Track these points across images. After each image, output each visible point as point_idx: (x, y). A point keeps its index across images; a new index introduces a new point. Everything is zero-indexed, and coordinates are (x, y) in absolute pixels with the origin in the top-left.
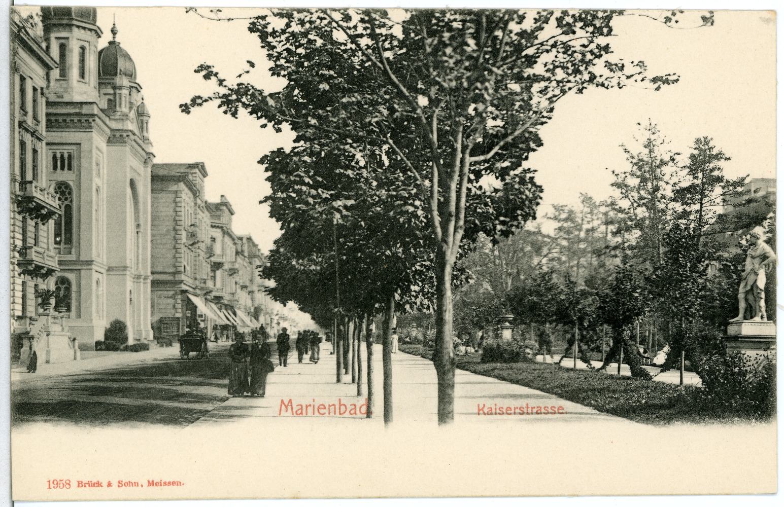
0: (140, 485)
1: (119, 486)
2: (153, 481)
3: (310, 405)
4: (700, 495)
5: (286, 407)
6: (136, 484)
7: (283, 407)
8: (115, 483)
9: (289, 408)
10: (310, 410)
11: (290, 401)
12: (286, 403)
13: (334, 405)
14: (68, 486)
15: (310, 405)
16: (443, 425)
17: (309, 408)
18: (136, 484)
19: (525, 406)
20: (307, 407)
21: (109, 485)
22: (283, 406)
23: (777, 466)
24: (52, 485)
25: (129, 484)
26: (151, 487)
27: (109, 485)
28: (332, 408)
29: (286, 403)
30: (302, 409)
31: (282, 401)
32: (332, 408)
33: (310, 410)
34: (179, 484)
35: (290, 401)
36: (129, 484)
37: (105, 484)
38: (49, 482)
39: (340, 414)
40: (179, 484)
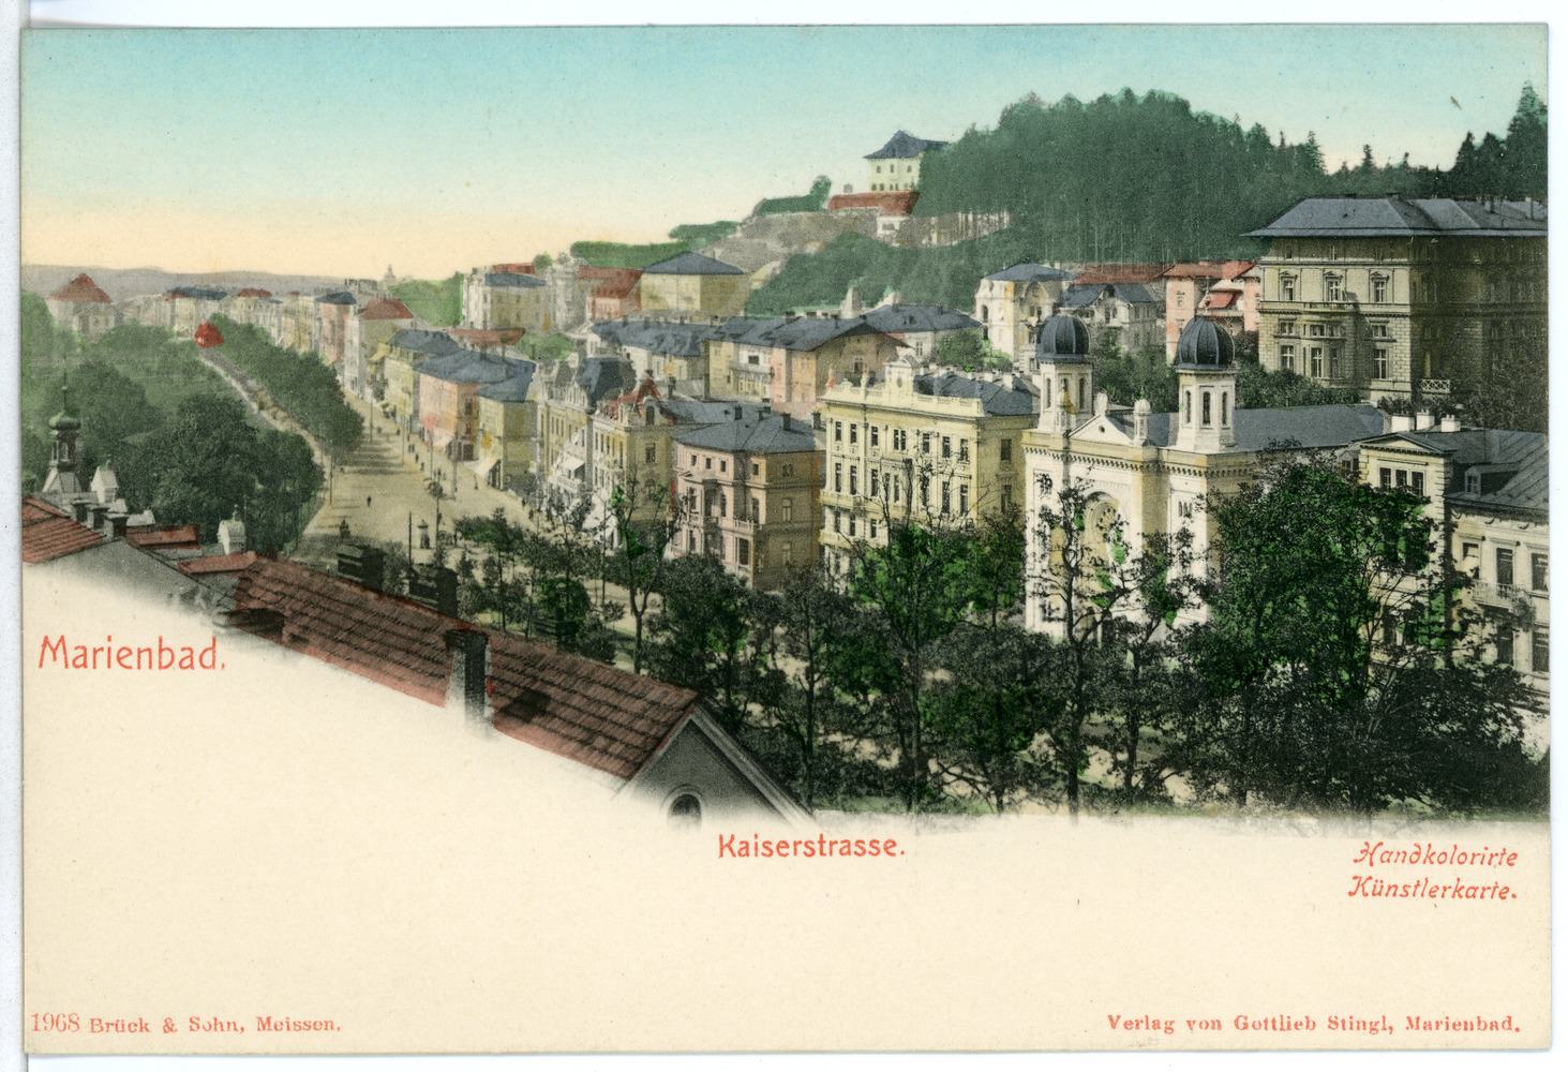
0: (335, 1027)
1: (192, 1029)
2: (268, 1019)
3: (102, 649)
4: (1256, 1051)
5: (54, 651)
6: (232, 1025)
7: (48, 652)
8: (181, 1024)
9: (60, 652)
10: (102, 657)
11: (62, 639)
12: (54, 644)
13: (149, 650)
14: (73, 1027)
15: (102, 649)
16: (679, 819)
17: (99, 654)
18: (232, 1025)
19: (816, 839)
20: (95, 651)
21: (169, 1027)
22: (48, 652)
23: (1550, 958)
24: (41, 1025)
25: (216, 1025)
26: (1413, 1031)
27: (169, 1027)
28: (145, 656)
29: (54, 644)
30: (85, 655)
31: (46, 642)
32: (145, 656)
33: (102, 657)
34: (328, 1025)
35: (62, 639)
36: (216, 1025)
37: (156, 1025)
38: (36, 1016)
39: (160, 667)
40: (328, 1025)
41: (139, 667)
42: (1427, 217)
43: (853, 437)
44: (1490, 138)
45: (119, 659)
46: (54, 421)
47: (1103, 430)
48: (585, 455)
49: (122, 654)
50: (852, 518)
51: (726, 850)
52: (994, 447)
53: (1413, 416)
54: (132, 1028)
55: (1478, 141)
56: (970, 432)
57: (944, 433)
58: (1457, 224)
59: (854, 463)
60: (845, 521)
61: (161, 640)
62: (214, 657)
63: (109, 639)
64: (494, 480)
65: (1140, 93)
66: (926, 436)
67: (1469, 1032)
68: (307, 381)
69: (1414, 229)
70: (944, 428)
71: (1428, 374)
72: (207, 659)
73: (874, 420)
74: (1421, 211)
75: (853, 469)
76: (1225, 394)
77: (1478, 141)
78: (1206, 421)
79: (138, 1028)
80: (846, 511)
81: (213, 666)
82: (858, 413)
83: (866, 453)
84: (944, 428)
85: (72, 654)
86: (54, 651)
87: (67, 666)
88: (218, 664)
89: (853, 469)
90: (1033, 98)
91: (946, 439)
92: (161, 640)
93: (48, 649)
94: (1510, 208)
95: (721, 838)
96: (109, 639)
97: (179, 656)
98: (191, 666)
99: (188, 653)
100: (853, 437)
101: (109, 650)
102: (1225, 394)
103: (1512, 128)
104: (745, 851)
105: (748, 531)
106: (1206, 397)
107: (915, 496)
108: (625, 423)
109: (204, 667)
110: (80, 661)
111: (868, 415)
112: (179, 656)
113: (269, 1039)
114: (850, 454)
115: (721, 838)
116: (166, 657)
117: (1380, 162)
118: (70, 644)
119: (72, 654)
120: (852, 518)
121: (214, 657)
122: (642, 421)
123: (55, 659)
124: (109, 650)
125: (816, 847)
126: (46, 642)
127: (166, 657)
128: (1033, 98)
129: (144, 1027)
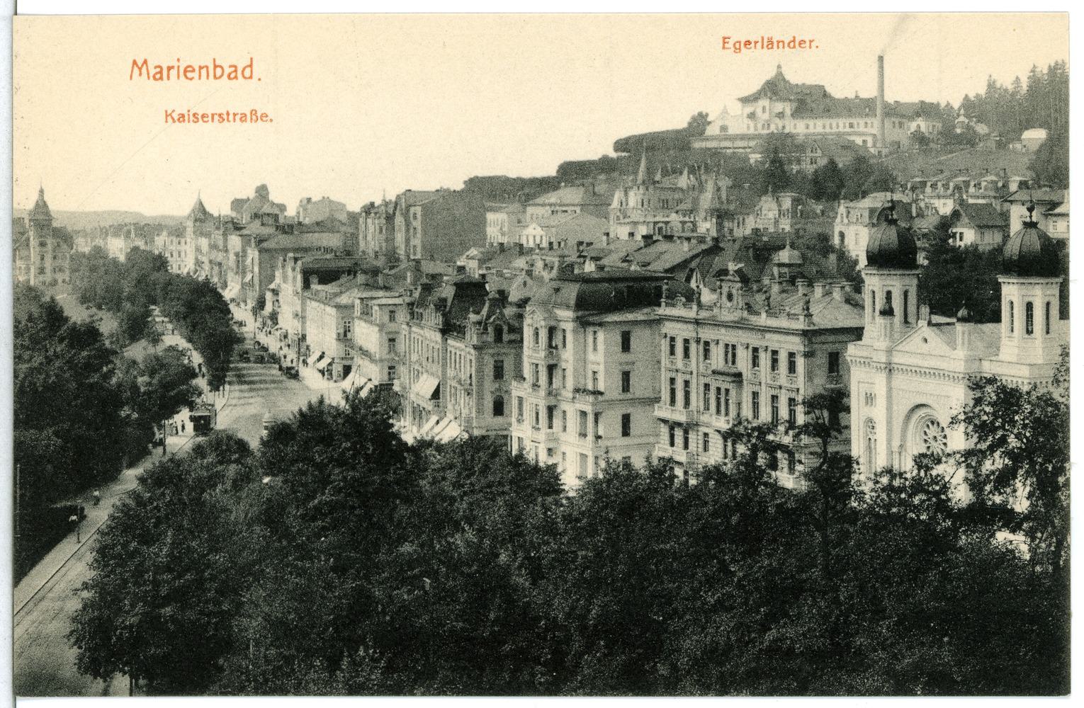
5: (140, 69)
7: (136, 69)
17: (172, 71)
28: (204, 72)
31: (135, 63)
35: (145, 62)
41: (200, 78)
43: (792, 368)
47: (926, 340)
48: (440, 373)
49: (189, 69)
50: (686, 432)
52: (822, 360)
56: (796, 344)
57: (775, 346)
59: (688, 377)
60: (679, 434)
62: (252, 71)
63: (178, 60)
66: (755, 350)
68: (202, 307)
70: (773, 341)
72: (247, 73)
73: (707, 334)
75: (687, 383)
76: (1048, 304)
78: (1029, 332)
80: (679, 424)
81: (251, 77)
82: (691, 327)
84: (773, 341)
85: (152, 71)
86: (140, 69)
87: (149, 78)
88: (255, 77)
89: (687, 383)
91: (775, 353)
92: (214, 60)
93: (136, 69)
96: (178, 60)
97: (227, 70)
98: (236, 77)
99: (233, 69)
100: (792, 368)
101: (179, 67)
102: (1048, 304)
106: (1029, 307)
107: (744, 406)
108: (475, 341)
109: (245, 78)
110: (158, 76)
111: (700, 330)
112: (227, 70)
114: (684, 369)
115: (166, 112)
116: (219, 71)
118: (151, 65)
119: (152, 71)
120: (686, 432)
121: (252, 71)
122: (490, 338)
123: (140, 74)
124: (179, 67)
125: (225, 117)
126: (135, 63)
127: (219, 71)
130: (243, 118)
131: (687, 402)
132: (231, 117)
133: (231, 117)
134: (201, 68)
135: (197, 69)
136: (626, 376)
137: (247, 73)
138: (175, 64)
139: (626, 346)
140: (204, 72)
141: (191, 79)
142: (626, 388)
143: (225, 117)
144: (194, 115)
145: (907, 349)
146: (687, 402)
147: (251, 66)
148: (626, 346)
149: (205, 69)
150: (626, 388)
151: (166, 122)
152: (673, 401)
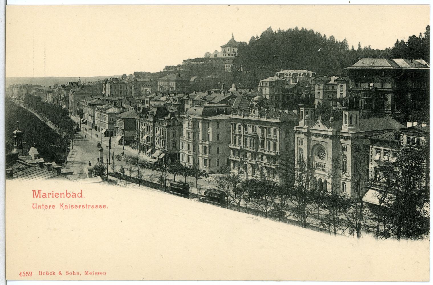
6: (78, 273)
8: (64, 273)
18: (78, 273)
21: (60, 273)
27: (60, 273)
37: (57, 273)
42: (396, 64)
44: (340, 42)
45: (55, 196)
46: (15, 132)
51: (61, 207)
53: (413, 122)
54: (51, 274)
55: (400, 40)
58: (404, 66)
61: (67, 191)
64: (121, 142)
65: (300, 29)
66: (263, 128)
67: (35, 203)
69: (393, 67)
71: (396, 108)
74: (394, 62)
77: (400, 40)
79: (52, 273)
83: (243, 133)
89: (162, 130)
90: (270, 29)
92: (67, 191)
94: (416, 61)
95: (60, 204)
97: (72, 194)
103: (250, 42)
104: (66, 207)
105: (207, 156)
109: (67, 197)
112: (72, 194)
113: (88, 277)
115: (60, 204)
117: (363, 47)
124: (53, 193)
125: (85, 206)
127: (68, 195)
128: (270, 29)
129: (54, 274)
130: (93, 207)
131: (240, 144)
132: (88, 207)
133: (88, 207)
134: (61, 194)
135: (60, 194)
136: (218, 137)
137: (80, 195)
138: (52, 193)
139: (218, 127)
140: (62, 195)
141: (57, 197)
142: (218, 139)
143: (85, 206)
144: (71, 206)
145: (313, 128)
146: (240, 144)
147: (81, 193)
148: (218, 127)
149: (63, 194)
150: (218, 139)
151: (60, 208)
152: (235, 143)
